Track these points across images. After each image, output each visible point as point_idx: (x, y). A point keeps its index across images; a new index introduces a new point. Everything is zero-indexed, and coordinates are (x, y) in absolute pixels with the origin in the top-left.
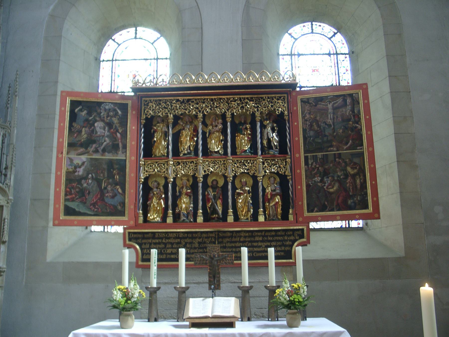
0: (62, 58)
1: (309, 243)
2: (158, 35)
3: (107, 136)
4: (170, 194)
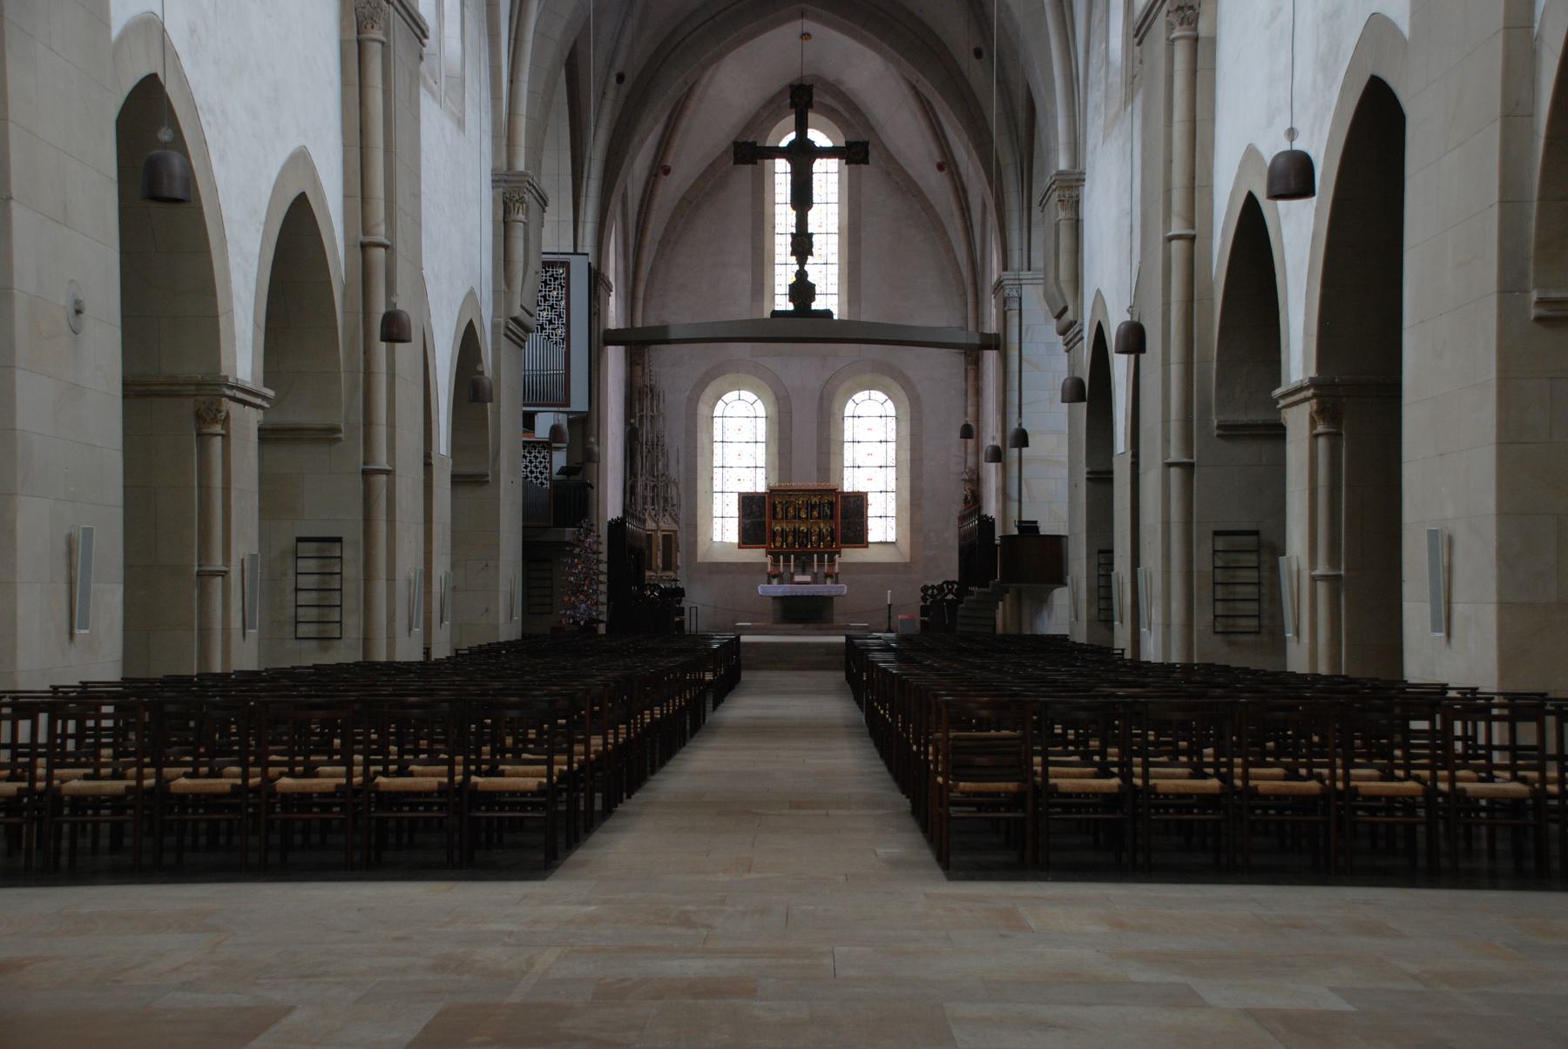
1: (1128, 311)
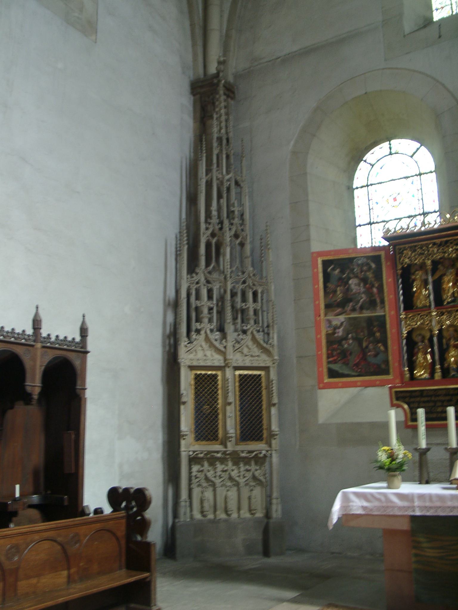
0: (310, 197)
2: (417, 145)
3: (364, 293)
4: (436, 348)
